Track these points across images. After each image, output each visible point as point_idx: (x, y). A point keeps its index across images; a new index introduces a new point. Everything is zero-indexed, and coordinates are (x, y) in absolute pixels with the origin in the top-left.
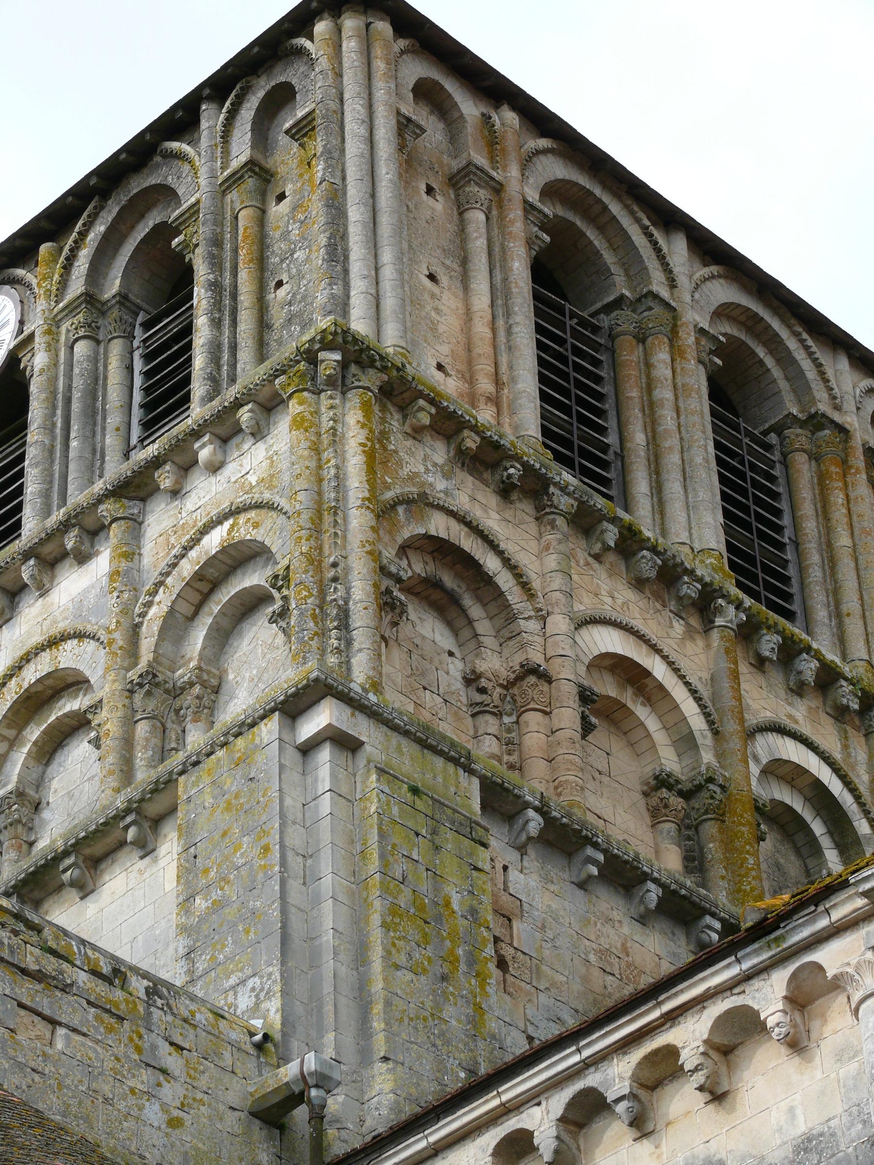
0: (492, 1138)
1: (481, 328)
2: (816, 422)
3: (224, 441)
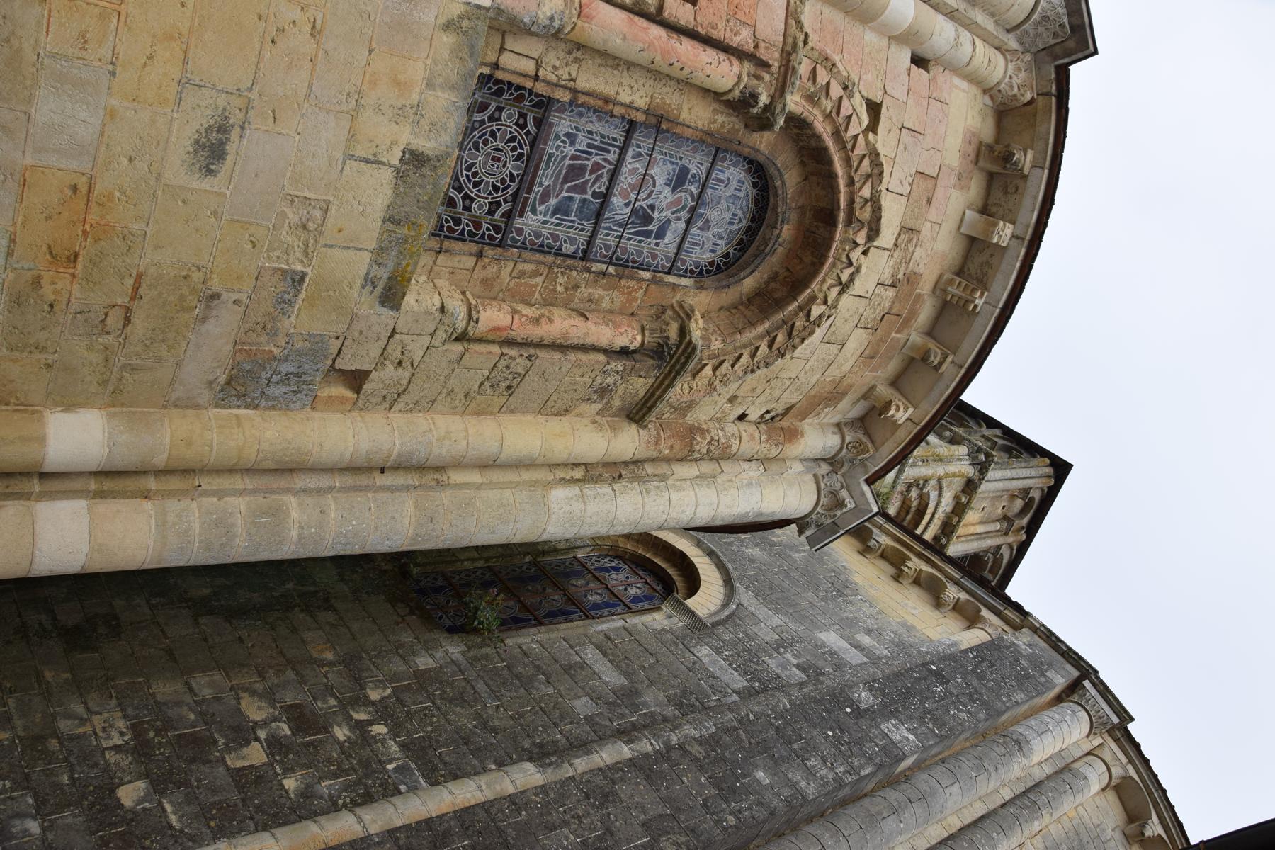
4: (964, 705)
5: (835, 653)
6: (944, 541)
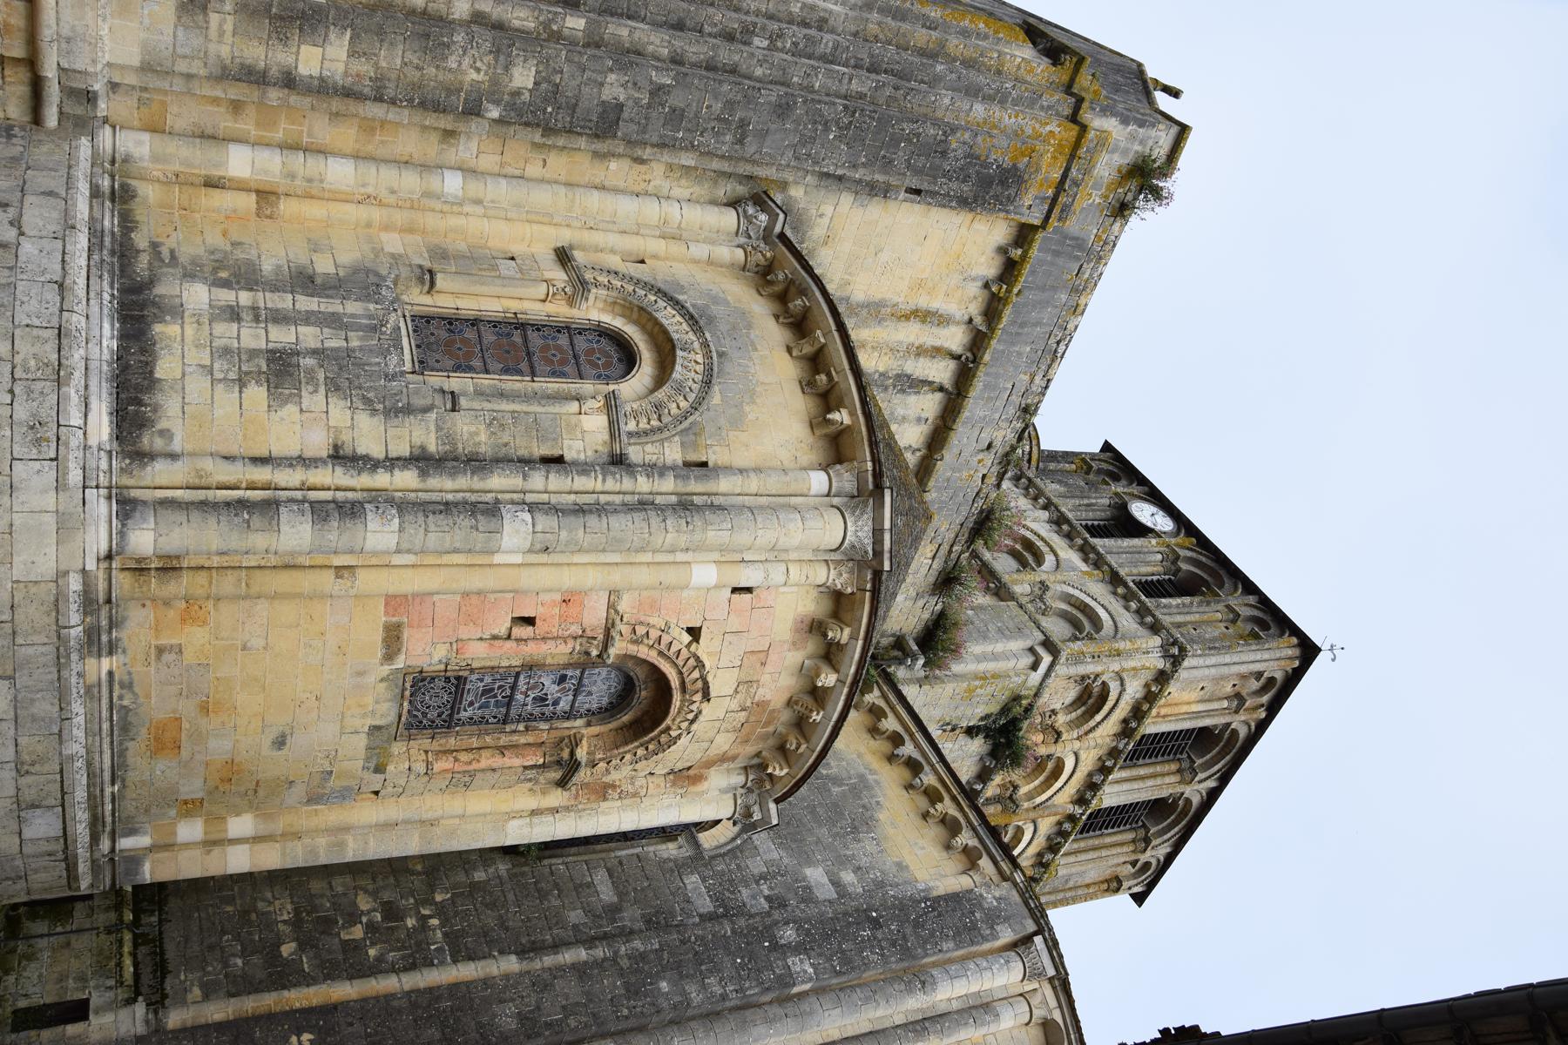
0: (900, 729)
1: (1185, 709)
2: (1147, 841)
3: (1137, 612)
4: (882, 949)
5: (809, 888)
6: (978, 787)
